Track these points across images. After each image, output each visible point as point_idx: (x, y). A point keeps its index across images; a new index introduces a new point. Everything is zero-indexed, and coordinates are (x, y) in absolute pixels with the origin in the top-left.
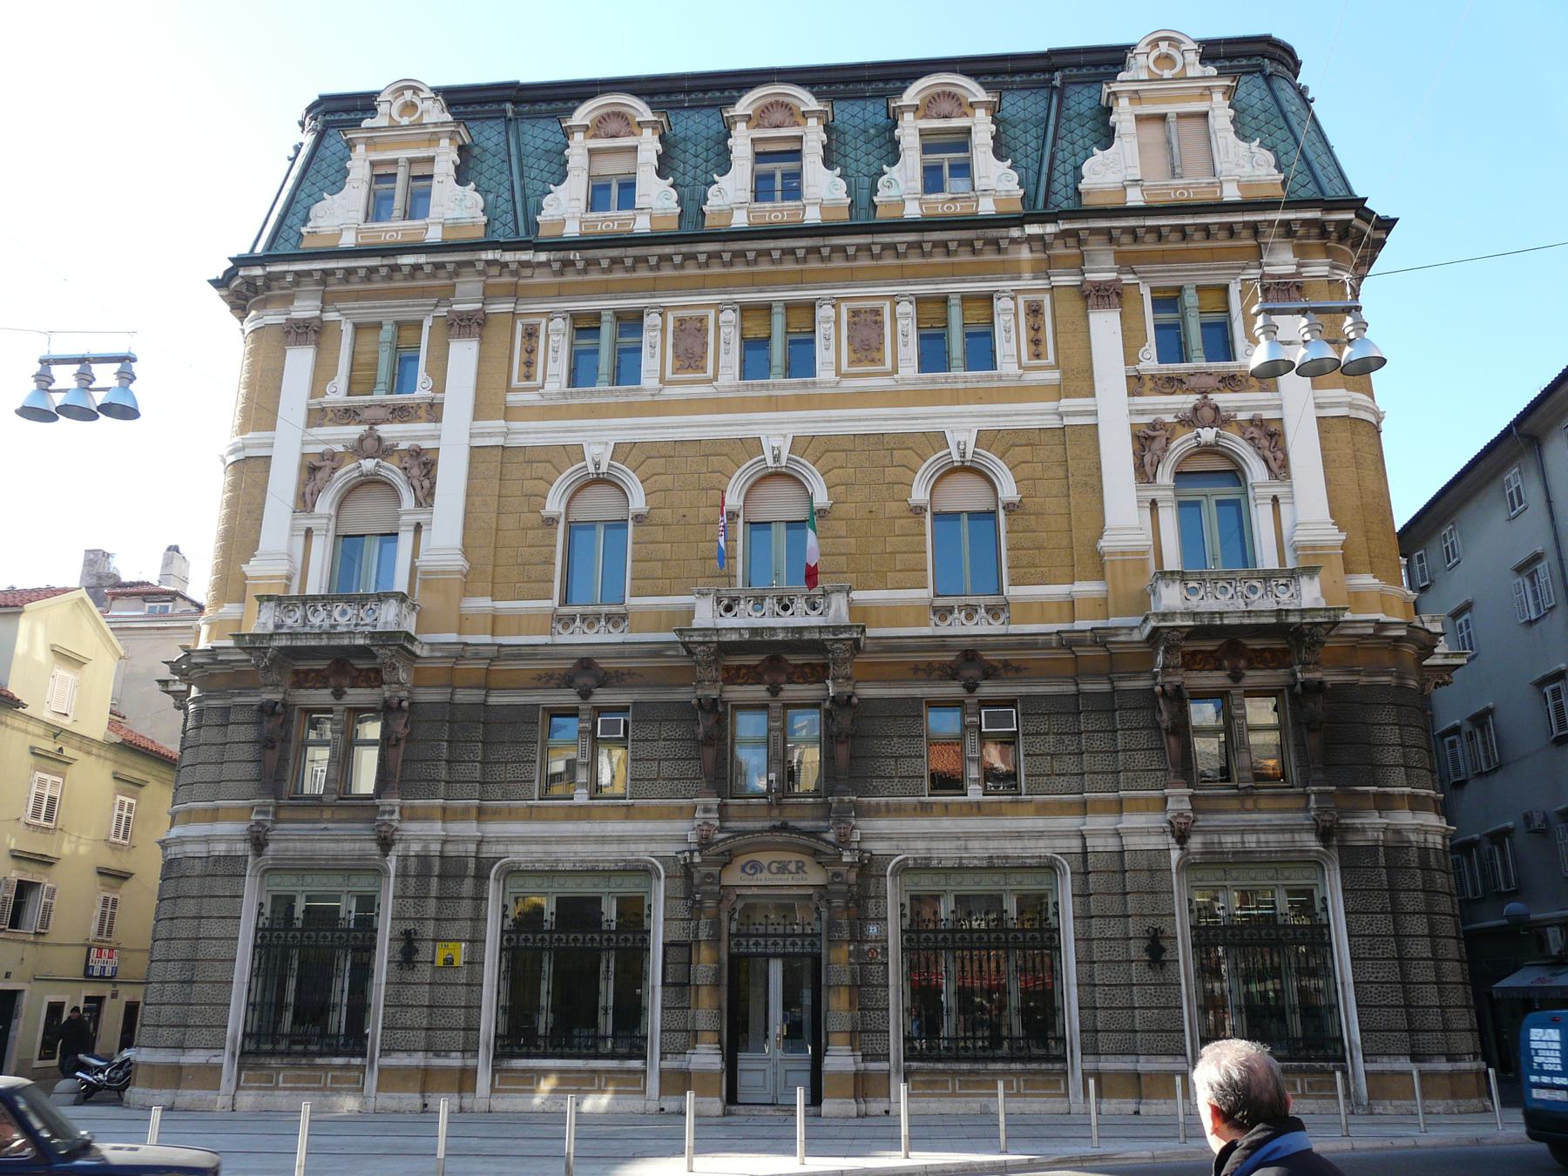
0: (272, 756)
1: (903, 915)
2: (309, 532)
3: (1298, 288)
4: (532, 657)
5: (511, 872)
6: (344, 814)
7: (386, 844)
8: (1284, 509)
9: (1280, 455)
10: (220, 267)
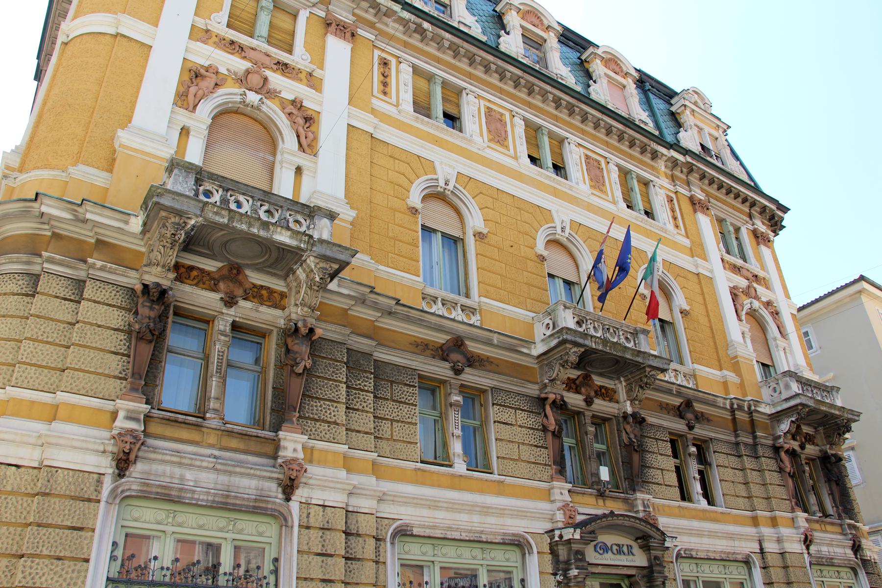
1: (113, 558)
2: (185, 132)
3: (353, 35)
4: (419, 322)
5: (403, 533)
6: (234, 443)
7: (289, 488)
8: (306, 178)
9: (310, 135)
10: (788, 220)
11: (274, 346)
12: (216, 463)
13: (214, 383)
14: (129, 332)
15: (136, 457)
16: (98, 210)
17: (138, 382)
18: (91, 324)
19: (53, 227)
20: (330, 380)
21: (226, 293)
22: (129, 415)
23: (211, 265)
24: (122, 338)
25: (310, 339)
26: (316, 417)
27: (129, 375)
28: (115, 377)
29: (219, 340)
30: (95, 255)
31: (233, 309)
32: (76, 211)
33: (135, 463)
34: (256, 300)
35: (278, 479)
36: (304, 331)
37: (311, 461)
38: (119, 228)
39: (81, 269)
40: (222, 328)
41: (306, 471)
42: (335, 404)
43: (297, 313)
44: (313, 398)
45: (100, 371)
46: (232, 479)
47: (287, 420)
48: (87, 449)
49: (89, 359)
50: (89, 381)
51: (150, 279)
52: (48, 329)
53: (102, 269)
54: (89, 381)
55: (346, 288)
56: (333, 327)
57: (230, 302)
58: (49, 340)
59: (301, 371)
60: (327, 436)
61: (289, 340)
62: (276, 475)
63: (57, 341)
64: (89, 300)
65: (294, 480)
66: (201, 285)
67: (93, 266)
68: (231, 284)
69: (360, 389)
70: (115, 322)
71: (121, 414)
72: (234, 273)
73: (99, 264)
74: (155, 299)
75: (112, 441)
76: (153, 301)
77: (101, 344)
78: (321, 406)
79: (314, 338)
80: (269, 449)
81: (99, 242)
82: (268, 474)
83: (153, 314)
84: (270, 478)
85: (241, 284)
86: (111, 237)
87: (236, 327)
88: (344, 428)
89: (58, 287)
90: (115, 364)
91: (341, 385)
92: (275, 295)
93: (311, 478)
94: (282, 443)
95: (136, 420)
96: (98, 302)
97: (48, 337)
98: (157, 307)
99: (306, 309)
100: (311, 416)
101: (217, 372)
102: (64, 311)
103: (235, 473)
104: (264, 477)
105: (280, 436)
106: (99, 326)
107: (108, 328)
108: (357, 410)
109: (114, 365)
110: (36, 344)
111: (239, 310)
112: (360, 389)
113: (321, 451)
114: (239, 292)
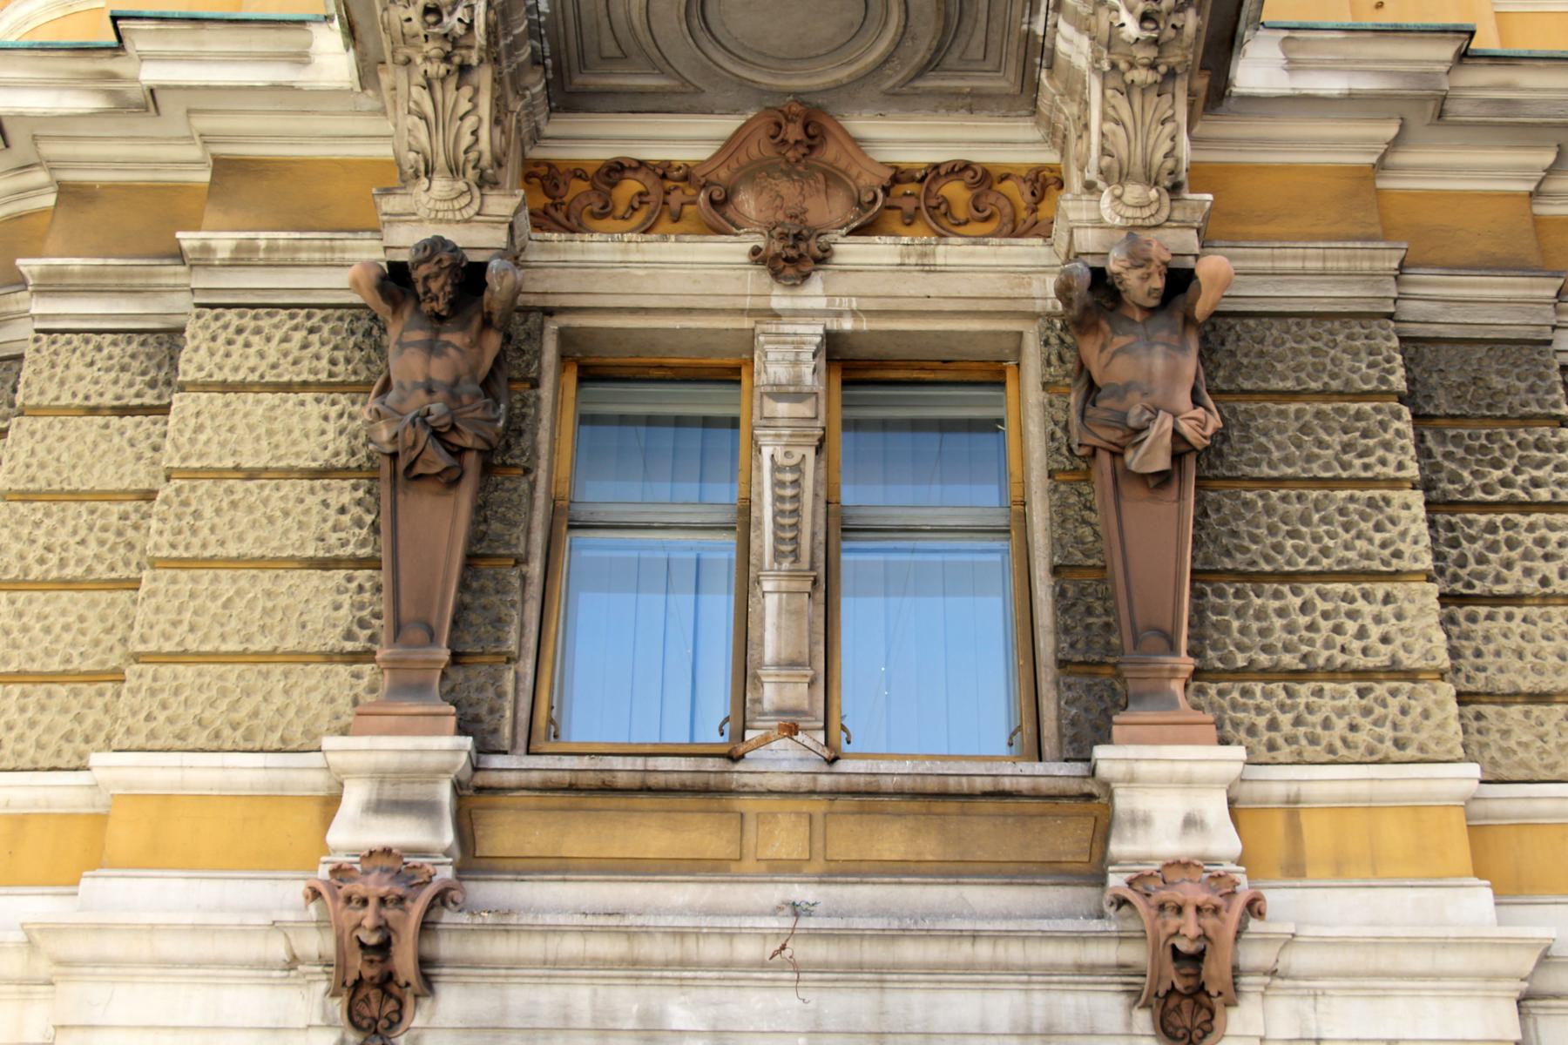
11: (1034, 395)
12: (792, 933)
13: (771, 602)
14: (364, 472)
15: (426, 963)
16: (182, 40)
17: (419, 654)
18: (217, 474)
19: (51, 166)
20: (1336, 483)
21: (770, 228)
22: (389, 792)
23: (688, 139)
24: (346, 498)
25: (1189, 320)
26: (1290, 660)
28: (330, 657)
29: (770, 422)
31: (816, 284)
32: (113, 76)
33: (428, 984)
34: (918, 227)
35: (1122, 968)
36: (1141, 286)
37: (1295, 869)
38: (275, 87)
39: (174, 289)
41: (1254, 908)
42: (1380, 589)
43: (1099, 224)
44: (1258, 578)
45: (262, 644)
46: (896, 1000)
47: (1140, 698)
48: (222, 963)
49: (214, 607)
50: (223, 692)
51: (405, 239)
52: (62, 535)
53: (242, 259)
54: (223, 692)
55: (1323, 67)
56: (1311, 257)
57: (794, 257)
58: (71, 571)
59: (1162, 462)
60: (1362, 738)
61: (1091, 350)
62: (1107, 953)
63: (101, 571)
64: (205, 387)
65: (1198, 958)
68: (786, 188)
69: (1512, 504)
71: (355, 795)
72: (800, 135)
73: (224, 242)
74: (440, 306)
75: (313, 910)
76: (438, 318)
77: (260, 542)
78: (1305, 608)
79: (1202, 309)
80: (1067, 841)
81: (225, 168)
82: (1067, 954)
83: (440, 370)
84: (1080, 969)
85: (833, 178)
86: (264, 136)
87: (852, 364)
88: (1447, 690)
91: (1396, 496)
92: (1008, 187)
94: (1123, 801)
95: (423, 809)
96: (241, 387)
97: (63, 563)
98: (456, 338)
99: (1133, 192)
100: (1264, 660)
101: (778, 555)
102: (106, 456)
103: (899, 968)
104: (1050, 969)
105: (1104, 769)
106: (252, 475)
107: (288, 473)
108: (1517, 599)
109: (319, 613)
110: (22, 597)
111: (843, 284)
112: (1512, 504)
113: (1342, 809)
114: (828, 209)
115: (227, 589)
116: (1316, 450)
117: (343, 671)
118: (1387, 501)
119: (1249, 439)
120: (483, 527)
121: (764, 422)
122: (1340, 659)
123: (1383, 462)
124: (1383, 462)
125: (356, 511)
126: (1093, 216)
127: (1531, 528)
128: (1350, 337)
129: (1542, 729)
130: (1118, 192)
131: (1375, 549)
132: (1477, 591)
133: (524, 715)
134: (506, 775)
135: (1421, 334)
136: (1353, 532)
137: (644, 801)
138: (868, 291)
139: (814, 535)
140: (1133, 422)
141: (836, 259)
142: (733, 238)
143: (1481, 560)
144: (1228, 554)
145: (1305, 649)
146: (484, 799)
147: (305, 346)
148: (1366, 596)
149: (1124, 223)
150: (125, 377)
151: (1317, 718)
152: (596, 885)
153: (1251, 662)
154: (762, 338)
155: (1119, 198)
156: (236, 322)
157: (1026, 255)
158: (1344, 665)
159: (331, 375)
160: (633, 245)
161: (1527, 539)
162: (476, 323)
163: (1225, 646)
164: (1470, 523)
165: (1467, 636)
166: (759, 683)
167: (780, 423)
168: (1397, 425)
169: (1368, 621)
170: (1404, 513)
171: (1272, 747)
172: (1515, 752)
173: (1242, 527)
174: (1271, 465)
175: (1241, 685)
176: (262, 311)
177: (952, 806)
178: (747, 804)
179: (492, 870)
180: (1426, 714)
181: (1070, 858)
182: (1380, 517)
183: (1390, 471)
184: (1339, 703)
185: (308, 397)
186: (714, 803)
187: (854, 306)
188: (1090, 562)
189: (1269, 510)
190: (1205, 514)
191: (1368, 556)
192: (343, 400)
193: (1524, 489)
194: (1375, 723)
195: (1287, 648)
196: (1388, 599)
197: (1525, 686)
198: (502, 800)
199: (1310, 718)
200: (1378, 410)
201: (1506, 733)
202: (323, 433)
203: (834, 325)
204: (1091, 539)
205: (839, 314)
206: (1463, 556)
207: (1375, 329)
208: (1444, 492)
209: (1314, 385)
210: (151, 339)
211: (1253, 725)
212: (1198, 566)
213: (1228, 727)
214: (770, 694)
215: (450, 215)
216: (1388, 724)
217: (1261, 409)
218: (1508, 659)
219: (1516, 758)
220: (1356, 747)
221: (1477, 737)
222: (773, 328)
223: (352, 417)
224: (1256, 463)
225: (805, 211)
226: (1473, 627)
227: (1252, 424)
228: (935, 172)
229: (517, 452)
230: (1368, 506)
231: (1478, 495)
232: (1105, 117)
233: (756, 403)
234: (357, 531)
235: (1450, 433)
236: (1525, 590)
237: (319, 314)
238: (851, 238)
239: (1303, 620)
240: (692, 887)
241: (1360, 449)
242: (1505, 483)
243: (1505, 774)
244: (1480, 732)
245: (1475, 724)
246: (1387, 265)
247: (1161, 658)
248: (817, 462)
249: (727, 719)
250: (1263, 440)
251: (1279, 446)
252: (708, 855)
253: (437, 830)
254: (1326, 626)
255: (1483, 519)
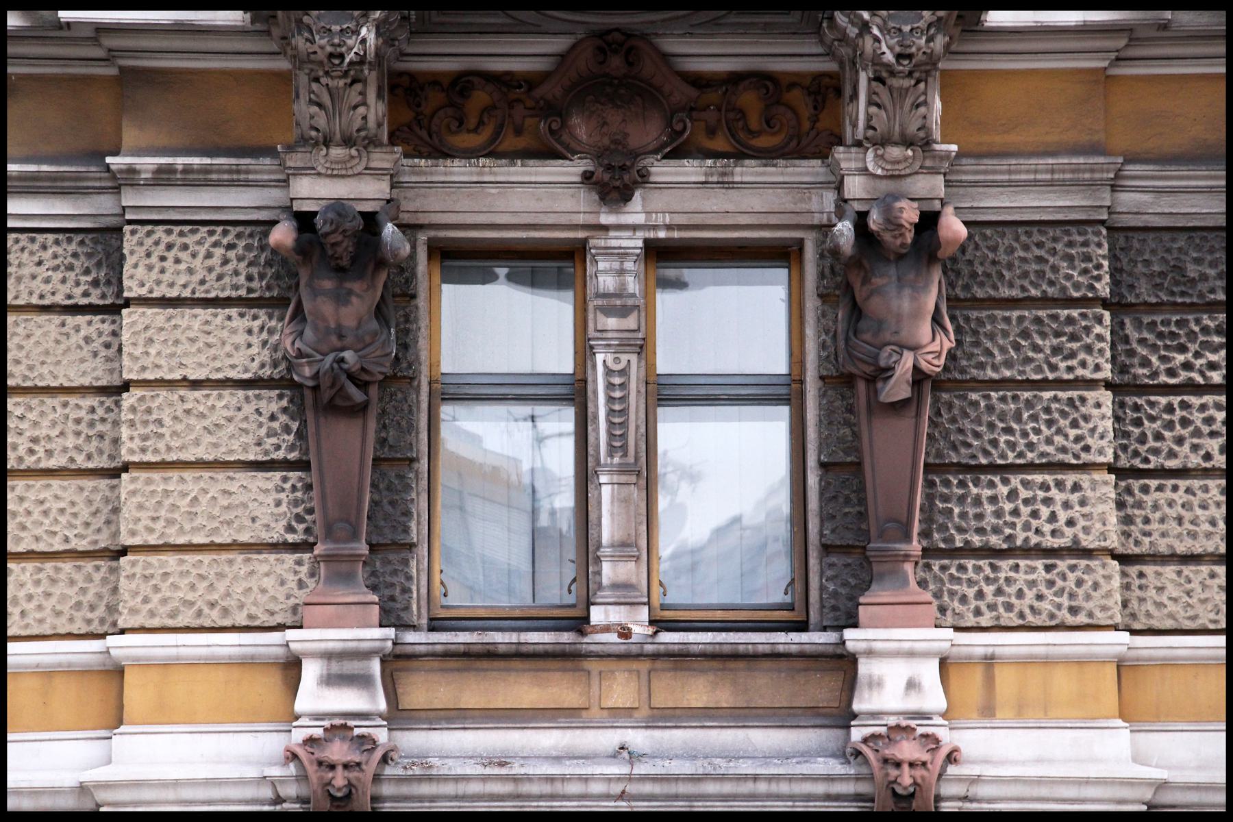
0: (349, 442)
6: (698, 691)
13: (606, 491)
20: (1044, 384)
22: (335, 667)
24: (274, 407)
26: (995, 541)
27: (317, 529)
28: (275, 547)
30: (130, 136)
40: (607, 282)
41: (952, 758)
42: (1070, 478)
43: (864, 171)
57: (615, 183)
59: (904, 392)
66: (510, 142)
67: (129, 178)
70: (240, 358)
73: (148, 163)
74: (345, 262)
75: (292, 769)
78: (1013, 495)
80: (821, 690)
89: (42, 272)
90: (264, 504)
91: (1091, 395)
93: (976, 780)
95: (360, 681)
100: (976, 540)
101: (612, 450)
106: (196, 384)
108: (1183, 473)
111: (659, 200)
113: (1026, 662)
114: (647, 131)
115: (193, 489)
116: (1030, 354)
117: (290, 558)
118: (1083, 400)
119: (977, 344)
120: (383, 435)
121: (599, 335)
122: (1035, 540)
123: (1083, 364)
124: (1083, 364)
125: (283, 418)
126: (860, 165)
127: (1203, 408)
128: (1071, 244)
129: (1189, 586)
130: (880, 152)
131: (1069, 445)
132: (1151, 466)
133: (424, 591)
134: (417, 647)
135: (1132, 224)
136: (1053, 429)
137: (517, 664)
138: (679, 209)
139: (637, 427)
140: (882, 363)
141: (652, 179)
142: (568, 162)
143: (1158, 437)
144: (954, 447)
145: (1008, 531)
146: (401, 664)
147: (226, 262)
148: (1060, 485)
149: (885, 173)
150: (71, 276)
151: (1012, 590)
152: (487, 732)
153: (967, 542)
154: (593, 251)
155: (882, 157)
156: (166, 239)
157: (807, 174)
158: (1037, 545)
159: (250, 290)
160: (487, 169)
161: (1197, 417)
162: (371, 267)
163: (947, 529)
164: (1152, 404)
165: (1139, 505)
166: (598, 560)
167: (610, 335)
168: (1098, 329)
169: (1058, 508)
170: (1095, 412)
171: (978, 612)
172: (1165, 606)
173: (967, 425)
174: (995, 368)
175: (957, 562)
176: (187, 228)
177: (741, 664)
178: (593, 666)
179: (410, 719)
180: (1096, 586)
181: (825, 705)
182: (1076, 415)
183: (1087, 373)
184: (1031, 577)
185: (234, 312)
186: (569, 664)
187: (668, 221)
188: (849, 459)
189: (990, 409)
190: (939, 414)
191: (1064, 450)
192: (262, 313)
193: (1202, 373)
194: (1055, 594)
195: (996, 530)
196: (1076, 487)
197: (1181, 548)
198: (415, 664)
199: (1007, 589)
200: (1084, 316)
201: (1160, 589)
202: (249, 346)
203: (651, 235)
204: (850, 438)
205: (655, 227)
206: (1144, 434)
207: (1091, 237)
208: (1135, 377)
209: (1034, 292)
210: (88, 238)
211: (965, 596)
212: (931, 460)
213: (946, 598)
214: (608, 572)
215: (344, 172)
216: (1066, 595)
217: (989, 317)
218: (1172, 526)
219: (1166, 611)
220: (1040, 614)
221: (1138, 593)
222: (602, 243)
223: (271, 332)
224: (981, 366)
225: (626, 135)
226: (1145, 498)
227: (982, 330)
228: (735, 79)
229: (404, 365)
230: (1067, 405)
231: (1163, 379)
232: (870, 103)
233: (591, 316)
234: (286, 437)
235: (1146, 319)
236: (1190, 465)
237: (234, 231)
238: (664, 161)
239: (1008, 507)
240: (556, 734)
241: (1065, 352)
242: (1187, 366)
243: (1156, 624)
244: (1140, 587)
245: (1137, 582)
246: (1105, 175)
247: (897, 546)
248: (639, 362)
249: (574, 580)
250: (989, 345)
251: (1003, 350)
252: (565, 706)
253: (373, 697)
254: (1025, 510)
255: (1163, 400)
